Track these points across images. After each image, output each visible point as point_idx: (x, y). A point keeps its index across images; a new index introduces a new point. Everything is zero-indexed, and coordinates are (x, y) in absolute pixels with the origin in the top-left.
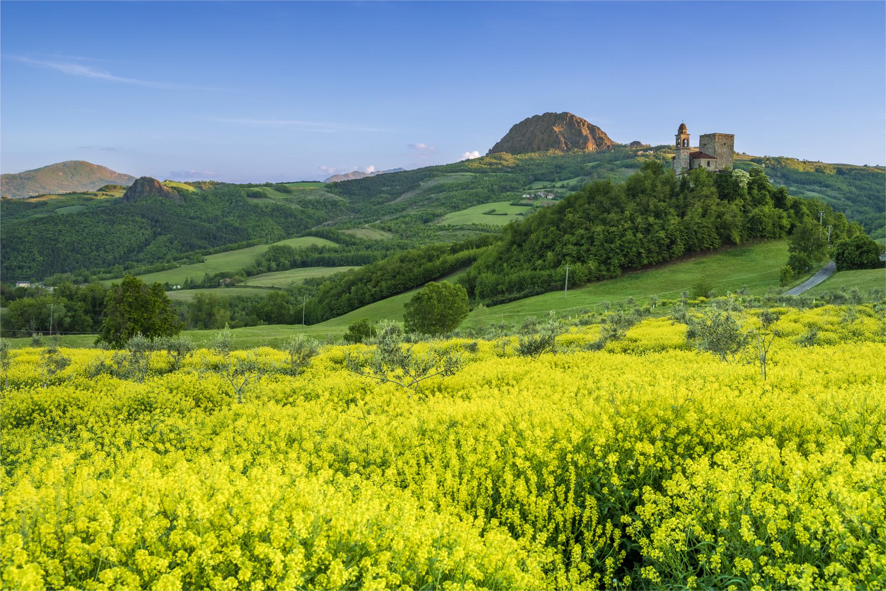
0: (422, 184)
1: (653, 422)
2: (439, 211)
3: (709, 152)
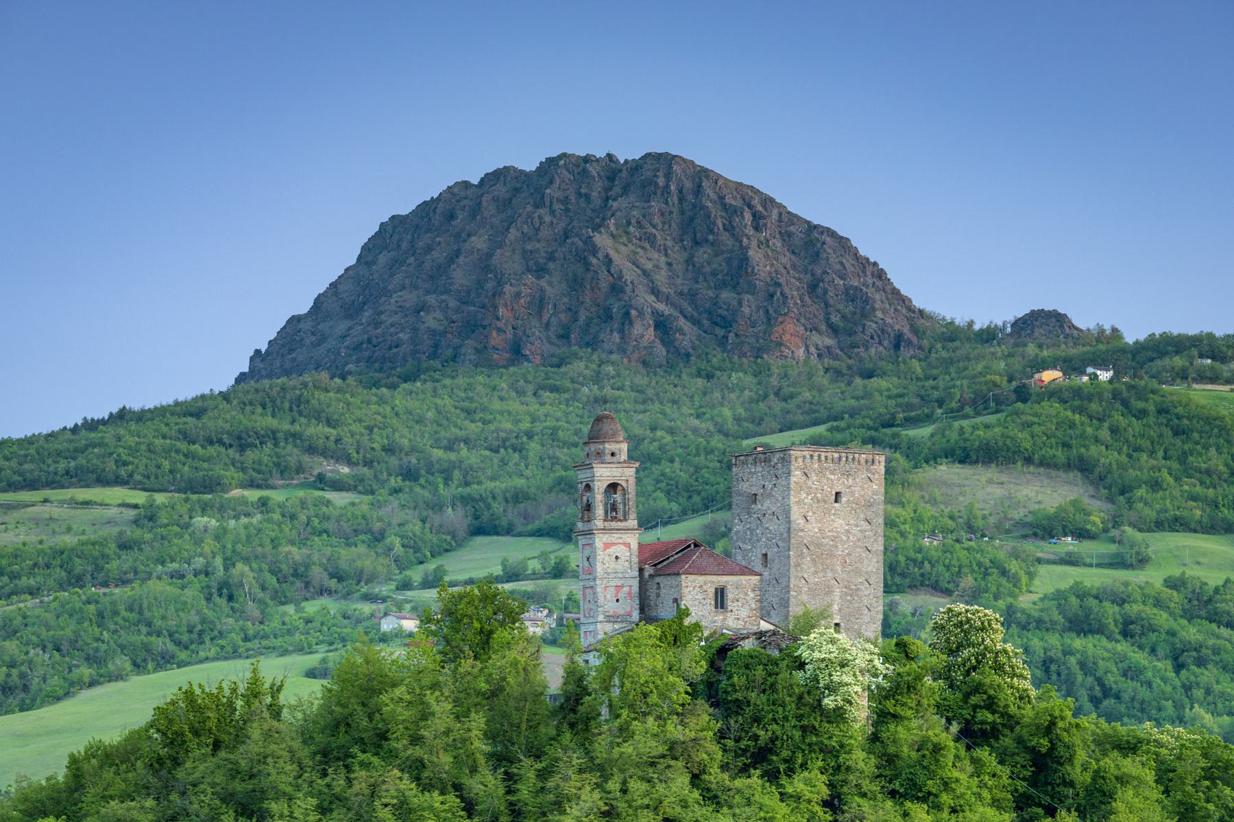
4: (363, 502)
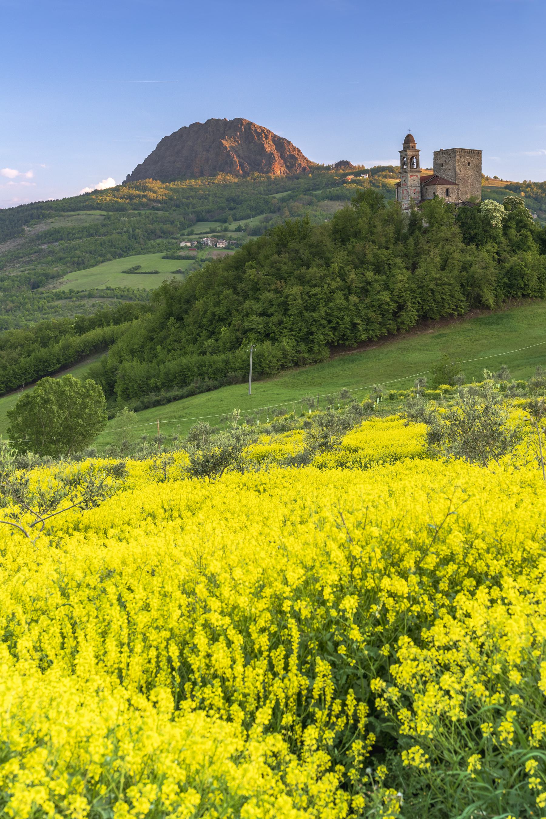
0: (26, 229)
1: (402, 551)
2: (54, 269)
3: (448, 175)
4: (167, 214)
